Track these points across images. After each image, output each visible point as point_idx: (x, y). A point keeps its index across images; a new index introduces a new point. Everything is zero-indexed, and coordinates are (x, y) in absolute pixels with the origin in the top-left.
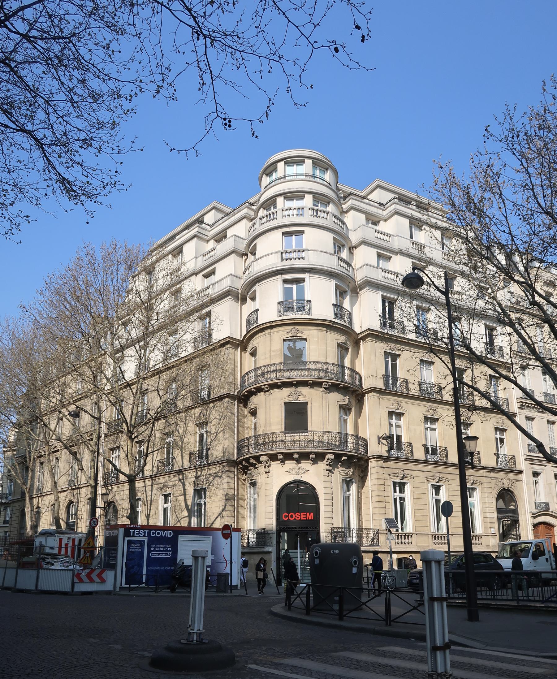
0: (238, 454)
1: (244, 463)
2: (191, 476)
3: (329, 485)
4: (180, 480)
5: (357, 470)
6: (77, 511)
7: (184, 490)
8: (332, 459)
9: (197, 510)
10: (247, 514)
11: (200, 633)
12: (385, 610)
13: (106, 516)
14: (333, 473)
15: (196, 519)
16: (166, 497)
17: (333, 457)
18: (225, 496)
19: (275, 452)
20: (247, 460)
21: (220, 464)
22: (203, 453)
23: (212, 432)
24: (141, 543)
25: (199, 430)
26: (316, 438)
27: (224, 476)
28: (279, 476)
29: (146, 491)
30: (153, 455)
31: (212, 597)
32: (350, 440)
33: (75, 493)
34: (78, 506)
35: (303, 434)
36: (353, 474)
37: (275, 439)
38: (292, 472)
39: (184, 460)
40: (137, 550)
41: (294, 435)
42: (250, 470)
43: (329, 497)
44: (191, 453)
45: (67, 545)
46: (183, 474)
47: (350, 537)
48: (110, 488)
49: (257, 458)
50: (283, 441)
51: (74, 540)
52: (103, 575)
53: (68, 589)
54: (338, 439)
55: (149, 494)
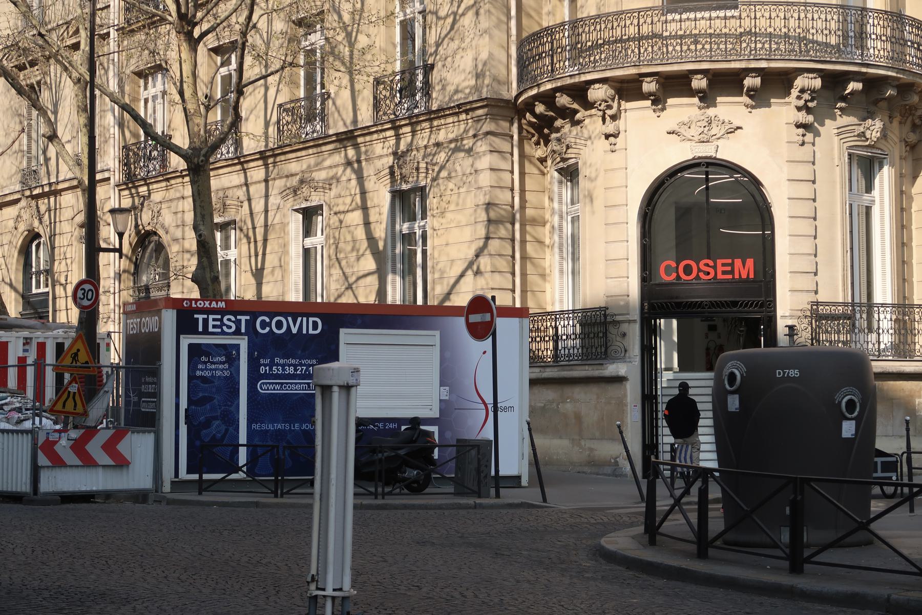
0: (520, 80)
1: (540, 108)
2: (381, 150)
3: (804, 172)
4: (349, 163)
5: (896, 123)
6: (52, 260)
7: (363, 193)
8: (813, 91)
9: (401, 254)
10: (552, 259)
11: (344, 598)
12: (546, 490)
13: (136, 274)
14: (817, 134)
15: (398, 279)
16: (309, 214)
17: (817, 83)
18: (487, 210)
19: (633, 71)
20: (548, 98)
21: (467, 112)
22: (415, 78)
23: (442, 13)
24: (230, 354)
25: (403, 8)
26: (763, 23)
27: (482, 147)
28: (643, 146)
29: (249, 200)
30: (267, 89)
31: (440, 507)
32: (875, 27)
33: (43, 208)
34: (53, 248)
35: (721, 14)
36: (884, 135)
37: (632, 31)
38: (688, 133)
39: (359, 102)
40: (219, 373)
41: (692, 15)
42: (558, 130)
43: (805, 209)
44: (378, 82)
45: (22, 360)
46: (356, 146)
47: (870, 330)
48: (143, 190)
49: (579, 92)
50: (660, 36)
51: (42, 347)
52: (122, 447)
53: (22, 485)
54: (833, 26)
55: (258, 206)
